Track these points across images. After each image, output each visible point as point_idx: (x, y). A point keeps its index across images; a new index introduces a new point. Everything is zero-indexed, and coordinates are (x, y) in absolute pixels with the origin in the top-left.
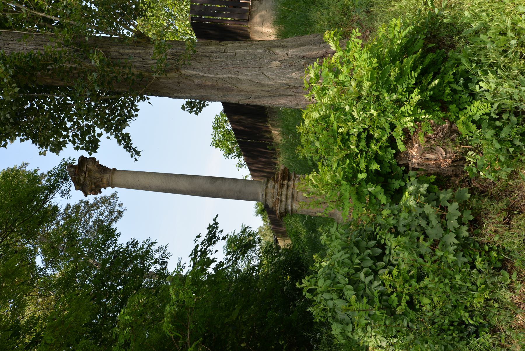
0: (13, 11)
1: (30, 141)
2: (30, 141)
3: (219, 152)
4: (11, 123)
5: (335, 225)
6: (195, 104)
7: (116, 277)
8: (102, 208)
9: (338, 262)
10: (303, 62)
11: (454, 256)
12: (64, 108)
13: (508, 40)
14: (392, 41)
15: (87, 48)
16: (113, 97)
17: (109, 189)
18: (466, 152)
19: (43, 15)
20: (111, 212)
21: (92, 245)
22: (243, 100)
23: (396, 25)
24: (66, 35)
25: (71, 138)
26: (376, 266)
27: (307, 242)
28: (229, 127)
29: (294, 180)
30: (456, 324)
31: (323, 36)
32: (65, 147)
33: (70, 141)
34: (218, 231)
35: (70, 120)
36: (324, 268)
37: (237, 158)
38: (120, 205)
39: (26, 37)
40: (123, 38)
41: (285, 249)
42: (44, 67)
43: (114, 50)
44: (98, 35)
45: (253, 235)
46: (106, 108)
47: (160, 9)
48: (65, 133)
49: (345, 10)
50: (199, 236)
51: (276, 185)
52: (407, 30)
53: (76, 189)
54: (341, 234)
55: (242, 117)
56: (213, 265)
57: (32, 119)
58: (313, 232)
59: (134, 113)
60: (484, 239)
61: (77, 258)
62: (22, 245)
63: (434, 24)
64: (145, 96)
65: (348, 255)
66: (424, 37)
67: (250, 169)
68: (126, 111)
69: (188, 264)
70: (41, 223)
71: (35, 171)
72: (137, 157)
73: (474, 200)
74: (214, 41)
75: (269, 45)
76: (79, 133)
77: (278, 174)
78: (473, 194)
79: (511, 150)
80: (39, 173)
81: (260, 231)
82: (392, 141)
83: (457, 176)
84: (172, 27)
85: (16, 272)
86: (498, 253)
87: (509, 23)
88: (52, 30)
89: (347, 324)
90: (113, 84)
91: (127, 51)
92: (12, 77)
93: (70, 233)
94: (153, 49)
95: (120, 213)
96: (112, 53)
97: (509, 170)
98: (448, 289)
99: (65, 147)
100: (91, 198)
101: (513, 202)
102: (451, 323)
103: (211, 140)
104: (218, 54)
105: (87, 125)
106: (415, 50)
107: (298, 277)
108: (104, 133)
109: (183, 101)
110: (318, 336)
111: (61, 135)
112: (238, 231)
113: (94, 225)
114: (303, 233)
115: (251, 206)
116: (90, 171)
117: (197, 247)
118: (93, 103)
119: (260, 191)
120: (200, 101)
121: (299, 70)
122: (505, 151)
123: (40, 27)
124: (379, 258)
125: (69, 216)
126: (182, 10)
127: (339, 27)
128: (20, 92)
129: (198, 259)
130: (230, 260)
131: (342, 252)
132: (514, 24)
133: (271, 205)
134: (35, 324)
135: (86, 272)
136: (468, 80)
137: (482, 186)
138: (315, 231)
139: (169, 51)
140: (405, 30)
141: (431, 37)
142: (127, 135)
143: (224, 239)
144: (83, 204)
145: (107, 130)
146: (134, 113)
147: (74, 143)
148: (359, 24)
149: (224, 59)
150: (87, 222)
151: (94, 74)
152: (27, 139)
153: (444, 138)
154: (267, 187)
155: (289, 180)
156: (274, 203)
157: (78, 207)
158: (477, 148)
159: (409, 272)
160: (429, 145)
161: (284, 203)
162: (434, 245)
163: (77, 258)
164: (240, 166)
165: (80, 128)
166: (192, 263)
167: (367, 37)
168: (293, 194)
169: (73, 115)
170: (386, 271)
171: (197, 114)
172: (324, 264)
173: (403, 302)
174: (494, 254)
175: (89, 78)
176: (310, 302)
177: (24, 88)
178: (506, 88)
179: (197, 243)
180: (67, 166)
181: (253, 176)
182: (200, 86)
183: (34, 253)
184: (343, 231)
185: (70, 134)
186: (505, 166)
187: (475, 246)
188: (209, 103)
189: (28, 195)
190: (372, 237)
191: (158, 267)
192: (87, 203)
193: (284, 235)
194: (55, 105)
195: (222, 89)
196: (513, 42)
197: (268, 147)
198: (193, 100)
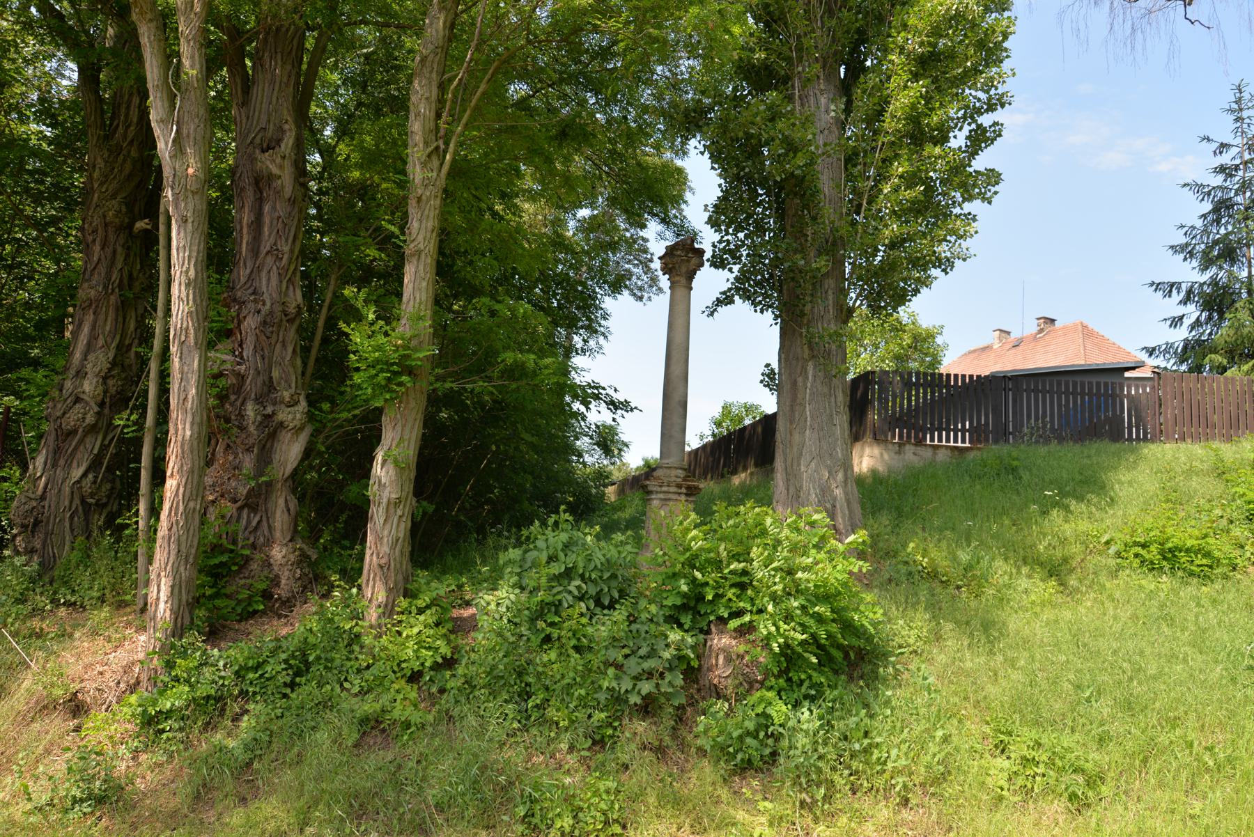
0: (865, 172)
1: (720, 194)
2: (720, 194)
3: (716, 412)
4: (739, 173)
5: (636, 550)
6: (773, 379)
7: (566, 298)
8: (645, 278)
9: (590, 555)
10: (829, 506)
11: (607, 688)
12: (761, 229)
13: (858, 740)
14: (856, 610)
15: (831, 253)
16: (777, 284)
17: (668, 283)
18: (727, 700)
19: (865, 203)
20: (641, 289)
21: (602, 269)
22: (779, 436)
23: (875, 613)
24: (844, 230)
25: (725, 238)
26: (588, 599)
27: (614, 520)
28: (747, 422)
29: (686, 501)
30: (528, 689)
31: (860, 528)
32: (716, 231)
33: (722, 237)
34: (623, 412)
35: (746, 237)
36: (584, 539)
37: (710, 433)
38: (650, 299)
39: (838, 186)
40: (845, 293)
41: (604, 494)
42: (806, 206)
43: (830, 283)
44: (847, 264)
45: (620, 456)
46: (763, 276)
47: (882, 335)
48: (731, 231)
49: (892, 553)
50: (616, 390)
51: (679, 480)
52: (869, 627)
53: (667, 247)
54: (625, 558)
55: (761, 437)
56: (583, 409)
57: (744, 195)
58: (626, 526)
59: (758, 308)
60: (626, 721)
61: (587, 253)
62: (601, 194)
63: (877, 657)
64: (779, 320)
65: (599, 566)
66: (862, 646)
67: (698, 449)
68: (760, 299)
69: (583, 379)
70: (626, 211)
71: (686, 202)
72: (706, 313)
73: (671, 710)
74: (848, 399)
75: (847, 465)
76: (732, 247)
77: (693, 481)
78: (678, 708)
79: (731, 750)
80: (683, 206)
81: (624, 464)
82: (739, 613)
83: (699, 690)
84: (862, 350)
85: (572, 188)
86: (611, 737)
87: (878, 740)
88: (848, 215)
89: (521, 567)
90: (791, 284)
91: (830, 298)
92: (792, 173)
93: (617, 243)
94: (835, 328)
95: (641, 298)
96: (827, 281)
97: (708, 748)
98: (567, 681)
99: (716, 231)
100: (656, 265)
101: (670, 753)
102: (527, 684)
103: (731, 401)
104: (833, 404)
105: (742, 255)
106: (847, 637)
107: (572, 509)
108: (734, 275)
109: (775, 366)
110: (506, 533)
111: (728, 227)
112: (623, 437)
113: (626, 270)
114: (626, 514)
115: (653, 452)
116: (688, 261)
117: (604, 389)
118: (767, 261)
119: (672, 461)
120: (777, 385)
121: (819, 501)
122: (730, 743)
123: (850, 201)
124: (598, 603)
125: (635, 242)
126: (883, 361)
127: (872, 547)
128: (775, 182)
129: (589, 391)
130: (589, 428)
131: (603, 560)
132: (877, 745)
133: (655, 474)
134: (514, 214)
135: (572, 264)
136: (812, 699)
137: (688, 718)
138: (627, 528)
139: (834, 347)
140: (869, 623)
141: (862, 655)
142: (732, 302)
143: (614, 420)
144: (649, 256)
145: (737, 279)
146: (758, 308)
147: (720, 242)
148: (875, 570)
149: (828, 412)
150: (629, 262)
151: (803, 262)
152: (722, 191)
153: (743, 674)
154: (677, 468)
155: (687, 495)
156: (658, 478)
157: (645, 251)
158: (732, 712)
159: (584, 636)
160: (734, 657)
161: (659, 489)
162: (619, 667)
163: (587, 253)
164: (702, 437)
165: (738, 247)
166: (585, 384)
167: (860, 581)
168: (669, 500)
169: (752, 240)
170: (584, 610)
171: (761, 382)
172: (589, 538)
173: (549, 630)
174: (610, 732)
175: (798, 256)
176: (544, 524)
177: (780, 186)
178: (802, 741)
179: (608, 389)
180: (693, 236)
181: (690, 453)
182: (794, 383)
183: (592, 205)
184: (628, 560)
185: (729, 237)
186: (712, 743)
187: (617, 711)
188: (775, 396)
189: (657, 196)
190: (622, 594)
191: (579, 346)
192: (651, 261)
193: (621, 492)
194: (762, 219)
195: (792, 411)
196: (857, 746)
197: (726, 469)
198: (777, 376)
